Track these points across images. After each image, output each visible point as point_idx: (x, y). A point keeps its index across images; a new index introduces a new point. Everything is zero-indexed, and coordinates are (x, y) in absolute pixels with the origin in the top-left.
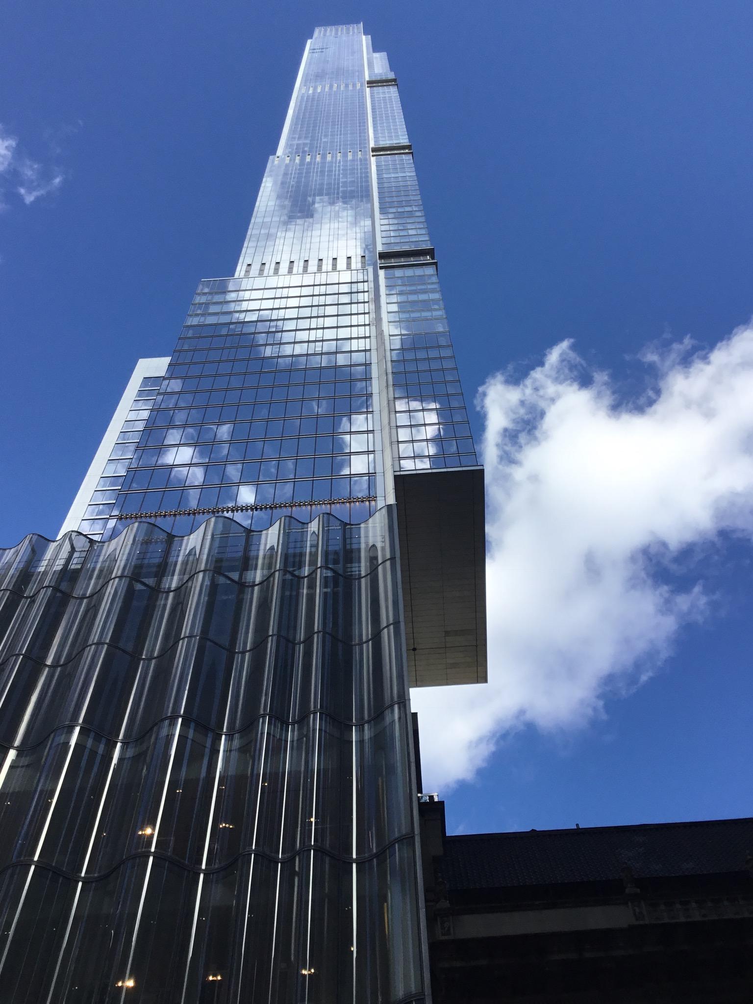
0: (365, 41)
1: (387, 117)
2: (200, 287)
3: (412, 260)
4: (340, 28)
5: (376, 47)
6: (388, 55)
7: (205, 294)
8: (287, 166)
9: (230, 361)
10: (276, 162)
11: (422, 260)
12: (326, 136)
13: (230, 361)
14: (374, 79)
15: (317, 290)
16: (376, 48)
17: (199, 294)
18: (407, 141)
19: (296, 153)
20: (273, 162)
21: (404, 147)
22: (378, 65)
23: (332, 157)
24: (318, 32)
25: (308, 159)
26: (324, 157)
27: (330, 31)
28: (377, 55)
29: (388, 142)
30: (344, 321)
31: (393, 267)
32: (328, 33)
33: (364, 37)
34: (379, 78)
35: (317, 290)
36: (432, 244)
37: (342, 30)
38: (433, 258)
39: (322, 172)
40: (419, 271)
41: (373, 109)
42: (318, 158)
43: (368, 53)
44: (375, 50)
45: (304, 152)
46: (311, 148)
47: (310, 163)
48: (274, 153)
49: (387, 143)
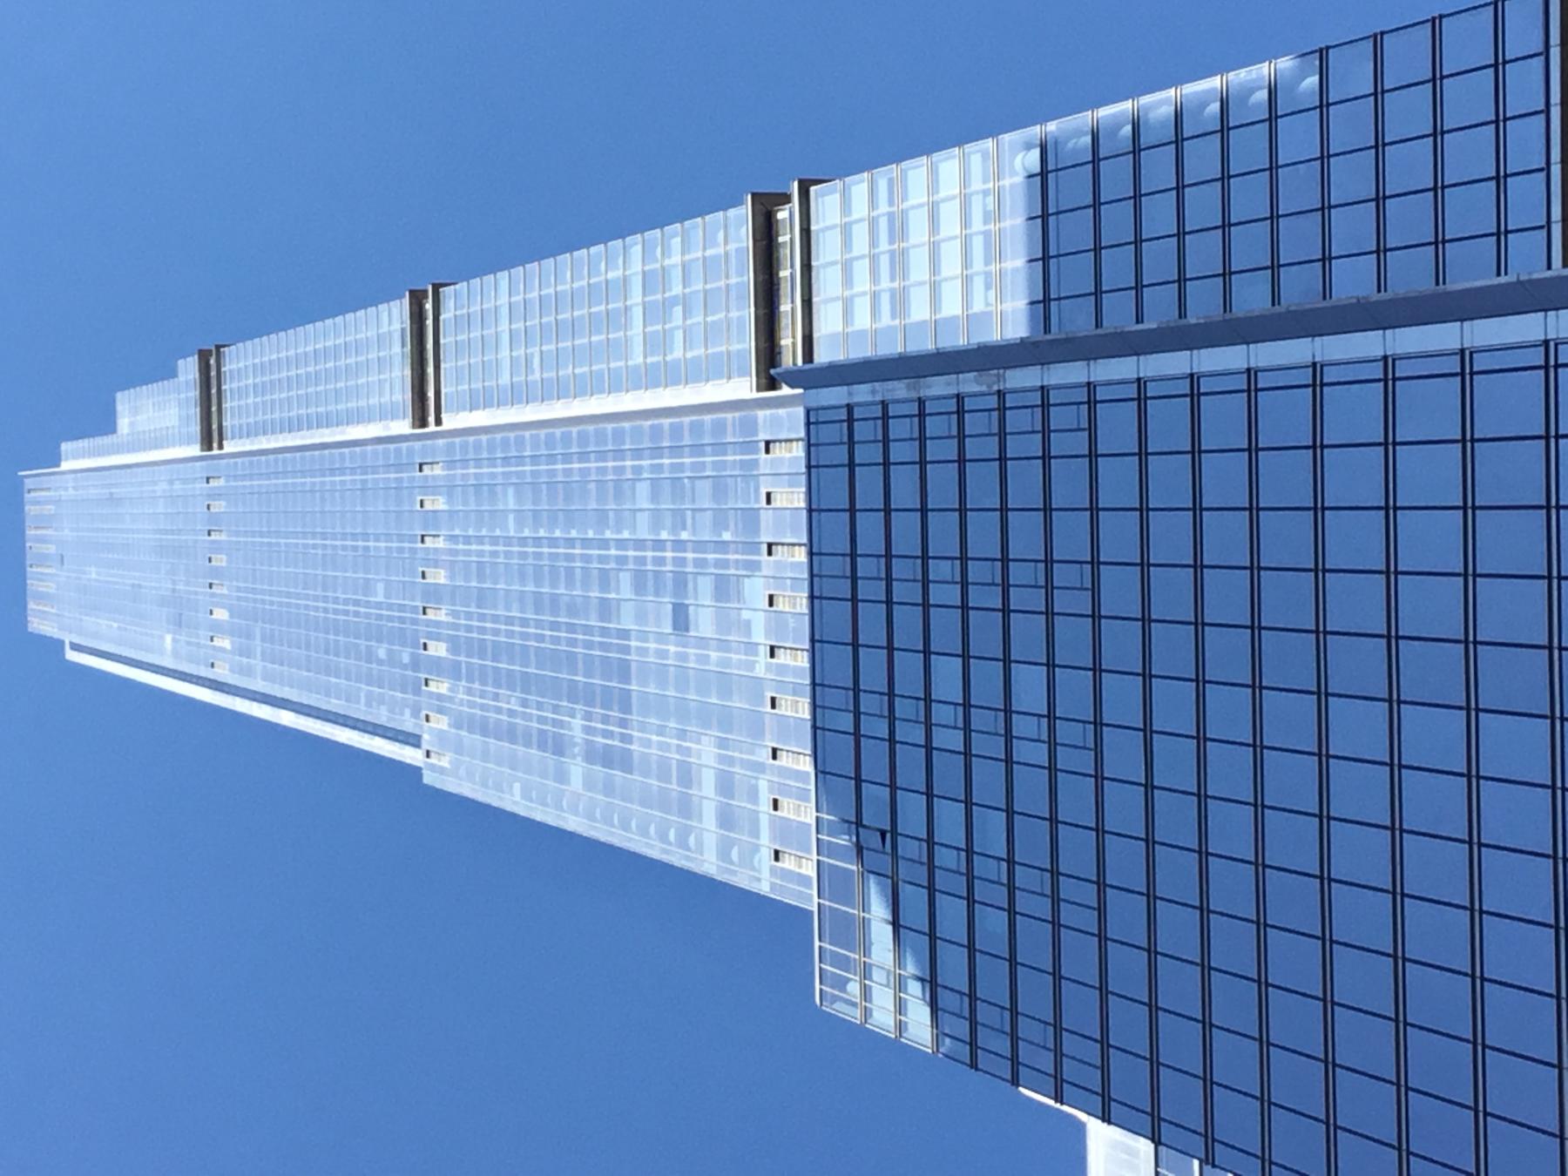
0: (76, 458)
1: (316, 378)
2: (840, 1010)
3: (789, 272)
4: (33, 548)
5: (99, 422)
6: (125, 387)
7: (866, 993)
8: (457, 725)
9: (1105, 1057)
10: (445, 762)
11: (789, 238)
12: (367, 587)
13: (1105, 1057)
14: (196, 428)
15: (871, 590)
16: (102, 423)
17: (867, 1013)
18: (395, 305)
19: (417, 692)
20: (442, 770)
21: (418, 317)
22: (156, 417)
23: (438, 638)
24: (42, 623)
25: (438, 649)
26: (435, 594)
27: (44, 580)
28: (124, 423)
29: (397, 349)
30: (989, 781)
31: (806, 232)
32: (49, 588)
33: (65, 466)
34: (195, 412)
35: (871, 590)
36: (737, 202)
37: (37, 502)
38: (786, 199)
39: (482, 598)
40: (826, 251)
41: (291, 426)
42: (440, 615)
43: (118, 449)
44: (107, 424)
45: (416, 664)
46: (401, 637)
47: (454, 648)
48: (416, 771)
49: (401, 373)
